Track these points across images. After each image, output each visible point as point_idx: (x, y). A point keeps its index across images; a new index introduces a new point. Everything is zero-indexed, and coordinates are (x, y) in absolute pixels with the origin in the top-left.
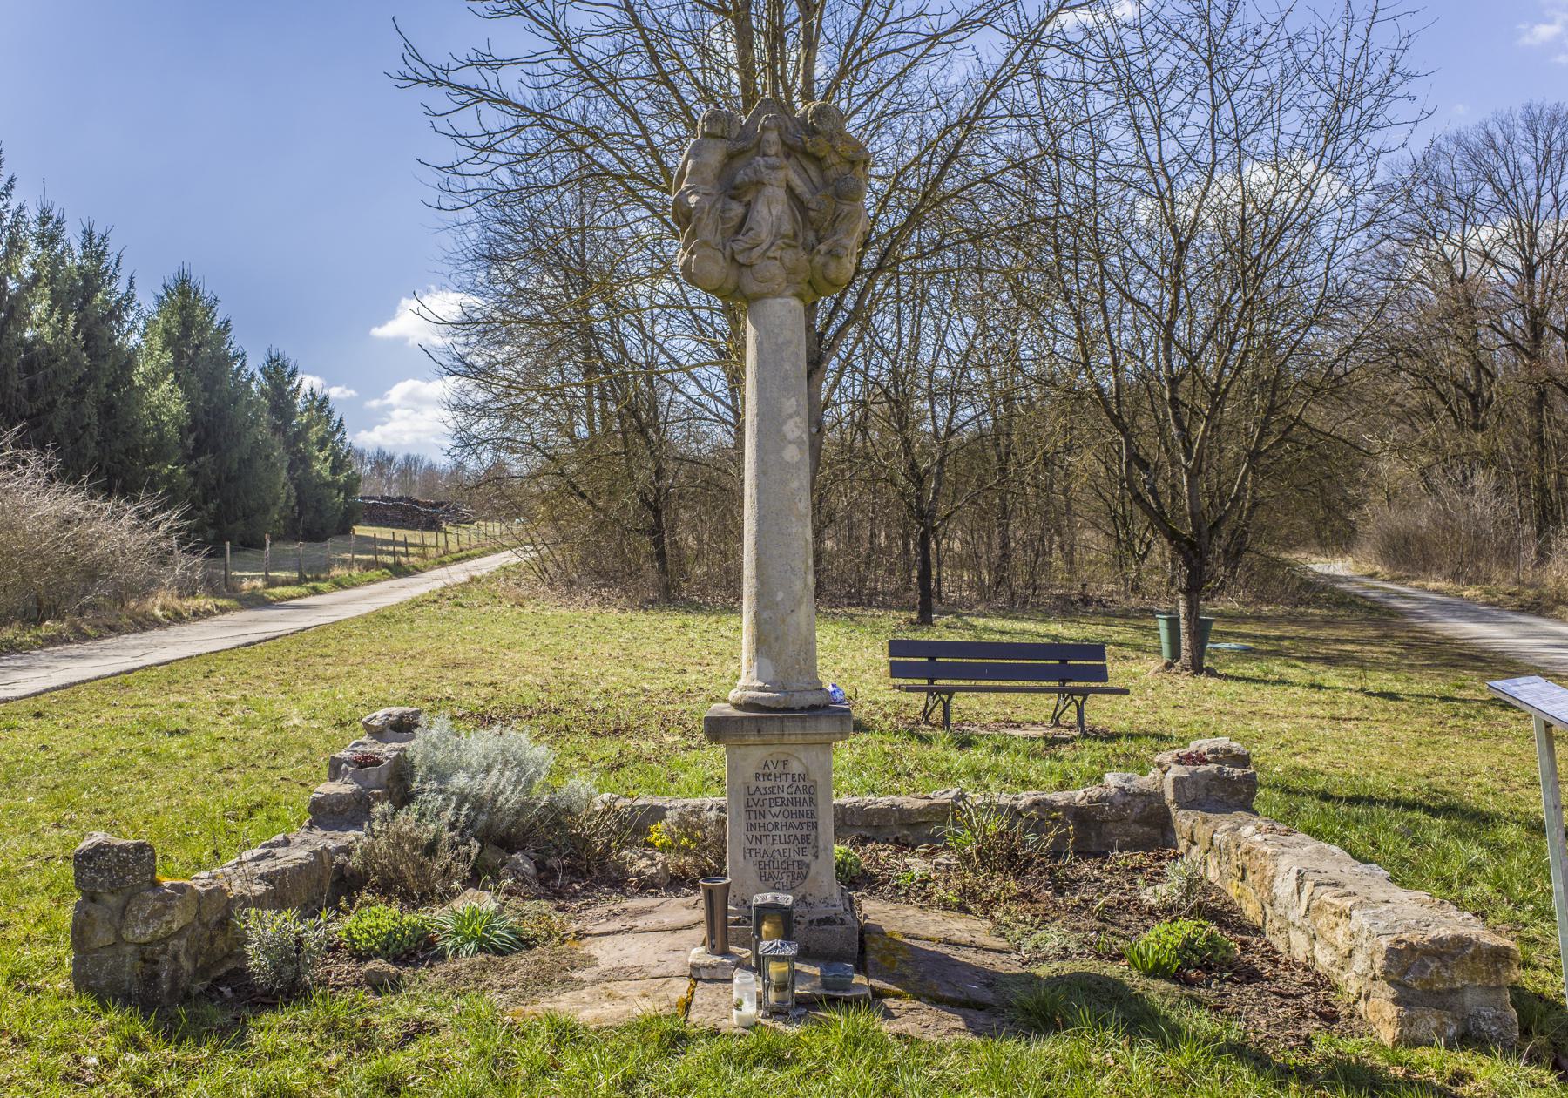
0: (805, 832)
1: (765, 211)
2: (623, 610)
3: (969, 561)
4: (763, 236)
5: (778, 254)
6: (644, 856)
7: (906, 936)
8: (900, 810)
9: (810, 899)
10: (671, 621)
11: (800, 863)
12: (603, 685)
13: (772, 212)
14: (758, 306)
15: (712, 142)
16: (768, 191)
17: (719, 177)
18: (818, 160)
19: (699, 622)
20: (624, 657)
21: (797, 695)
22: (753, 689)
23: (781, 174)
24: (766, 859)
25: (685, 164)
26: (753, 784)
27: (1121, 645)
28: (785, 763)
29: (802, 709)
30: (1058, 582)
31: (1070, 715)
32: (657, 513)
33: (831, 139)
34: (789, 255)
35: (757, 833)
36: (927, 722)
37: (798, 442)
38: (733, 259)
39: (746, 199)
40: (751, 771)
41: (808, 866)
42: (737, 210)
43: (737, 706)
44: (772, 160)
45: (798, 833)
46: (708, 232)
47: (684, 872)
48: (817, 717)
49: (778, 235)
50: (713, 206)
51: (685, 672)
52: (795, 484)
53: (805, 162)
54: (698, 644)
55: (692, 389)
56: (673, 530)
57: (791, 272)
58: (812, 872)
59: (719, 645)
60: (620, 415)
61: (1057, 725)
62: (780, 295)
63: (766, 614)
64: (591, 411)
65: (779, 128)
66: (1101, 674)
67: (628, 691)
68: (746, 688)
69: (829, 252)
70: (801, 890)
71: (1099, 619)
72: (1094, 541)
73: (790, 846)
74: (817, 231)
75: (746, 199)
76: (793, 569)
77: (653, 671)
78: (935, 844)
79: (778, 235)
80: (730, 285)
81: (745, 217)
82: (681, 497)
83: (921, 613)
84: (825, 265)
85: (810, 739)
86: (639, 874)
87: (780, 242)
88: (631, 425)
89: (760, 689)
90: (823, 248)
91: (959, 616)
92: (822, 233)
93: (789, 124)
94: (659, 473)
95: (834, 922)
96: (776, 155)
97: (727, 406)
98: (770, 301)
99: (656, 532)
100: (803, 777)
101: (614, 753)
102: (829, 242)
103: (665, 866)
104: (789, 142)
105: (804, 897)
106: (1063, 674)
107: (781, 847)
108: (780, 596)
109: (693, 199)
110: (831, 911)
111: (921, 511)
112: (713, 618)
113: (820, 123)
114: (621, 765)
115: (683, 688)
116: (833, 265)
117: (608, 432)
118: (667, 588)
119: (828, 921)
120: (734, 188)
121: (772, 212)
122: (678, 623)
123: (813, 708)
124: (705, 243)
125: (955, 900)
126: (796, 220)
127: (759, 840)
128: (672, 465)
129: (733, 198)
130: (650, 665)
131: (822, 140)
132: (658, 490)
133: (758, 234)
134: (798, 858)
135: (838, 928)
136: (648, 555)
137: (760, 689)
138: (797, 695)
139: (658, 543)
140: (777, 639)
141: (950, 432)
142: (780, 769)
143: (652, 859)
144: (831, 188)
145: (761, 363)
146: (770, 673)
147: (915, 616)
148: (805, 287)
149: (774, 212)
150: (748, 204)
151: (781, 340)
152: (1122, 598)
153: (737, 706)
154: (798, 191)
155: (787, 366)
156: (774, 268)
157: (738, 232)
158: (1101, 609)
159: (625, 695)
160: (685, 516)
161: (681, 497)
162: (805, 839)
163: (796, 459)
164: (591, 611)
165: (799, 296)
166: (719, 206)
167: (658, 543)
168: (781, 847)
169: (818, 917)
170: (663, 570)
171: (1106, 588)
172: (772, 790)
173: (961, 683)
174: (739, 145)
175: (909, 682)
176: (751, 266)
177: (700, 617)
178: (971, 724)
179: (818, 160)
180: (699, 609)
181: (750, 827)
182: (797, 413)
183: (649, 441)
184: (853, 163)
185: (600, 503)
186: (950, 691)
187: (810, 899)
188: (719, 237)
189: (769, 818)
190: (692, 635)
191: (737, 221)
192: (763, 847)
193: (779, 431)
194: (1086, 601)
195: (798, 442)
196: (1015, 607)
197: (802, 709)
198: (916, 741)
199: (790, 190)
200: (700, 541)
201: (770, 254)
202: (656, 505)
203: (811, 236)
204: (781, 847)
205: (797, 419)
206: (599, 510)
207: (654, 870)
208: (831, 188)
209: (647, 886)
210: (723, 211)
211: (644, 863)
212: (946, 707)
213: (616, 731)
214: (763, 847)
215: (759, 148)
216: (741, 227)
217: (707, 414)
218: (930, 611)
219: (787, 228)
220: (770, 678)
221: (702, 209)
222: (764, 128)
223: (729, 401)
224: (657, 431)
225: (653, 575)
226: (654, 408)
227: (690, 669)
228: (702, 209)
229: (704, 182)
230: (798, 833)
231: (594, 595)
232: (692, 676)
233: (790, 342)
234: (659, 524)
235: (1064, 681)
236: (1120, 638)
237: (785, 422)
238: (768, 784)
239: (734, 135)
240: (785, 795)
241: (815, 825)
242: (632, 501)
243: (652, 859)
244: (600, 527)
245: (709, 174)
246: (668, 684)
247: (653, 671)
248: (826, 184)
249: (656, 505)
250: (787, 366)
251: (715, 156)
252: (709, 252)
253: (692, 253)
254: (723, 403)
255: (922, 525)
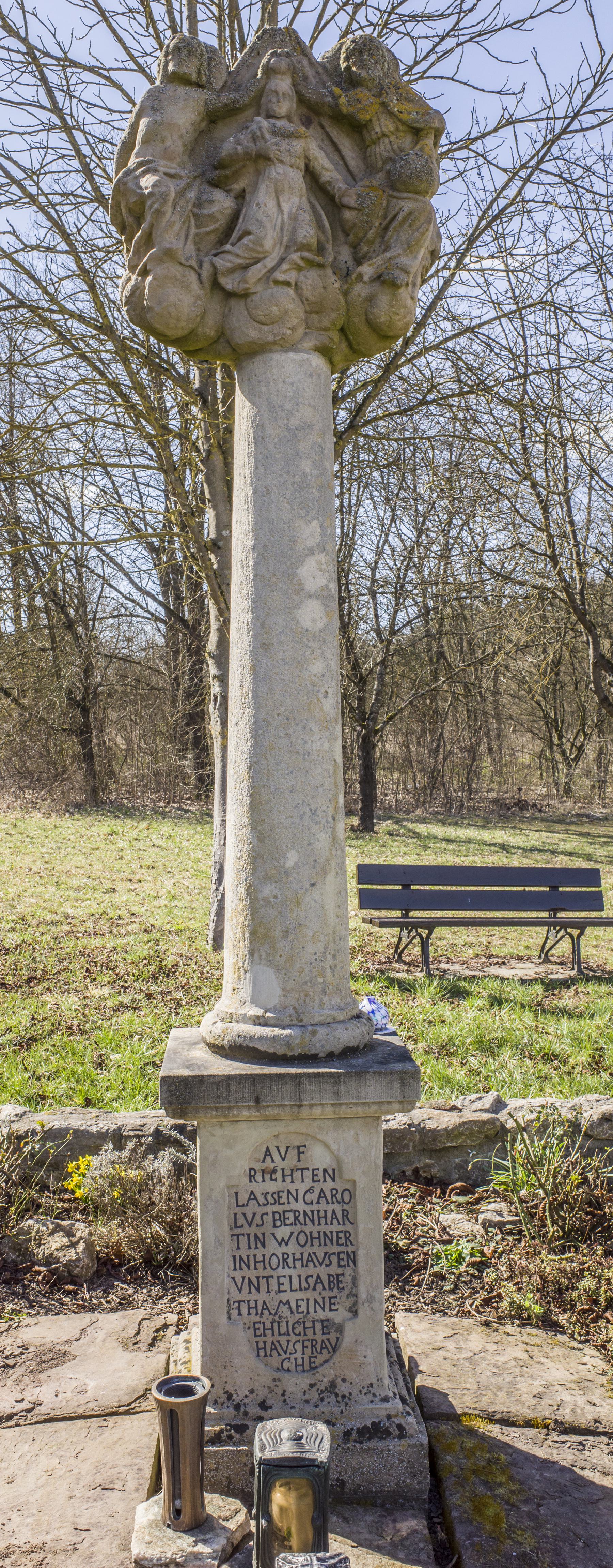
0: (334, 1269)
1: (271, 204)
2: (48, 815)
3: (406, 764)
4: (268, 244)
5: (292, 276)
6: (58, 1228)
7: (491, 1418)
8: (422, 1131)
9: (343, 1388)
10: (96, 828)
11: (327, 1325)
12: (20, 909)
13: (279, 207)
14: (257, 365)
15: (181, 90)
16: (276, 171)
17: (191, 150)
18: (357, 128)
19: (128, 828)
20: (48, 874)
21: (322, 1031)
22: (245, 1019)
23: (298, 146)
24: (267, 1318)
25: (134, 128)
26: (245, 1186)
27: (571, 854)
28: (300, 1150)
29: (330, 1057)
30: (488, 789)
31: (564, 947)
32: (85, 711)
33: (381, 91)
34: (311, 280)
35: (252, 1274)
36: (400, 960)
37: (321, 595)
38: (216, 284)
39: (237, 187)
40: (242, 1165)
41: (340, 1329)
42: (222, 202)
43: (217, 1049)
44: (281, 124)
45: (323, 1272)
46: (173, 235)
47: (118, 1254)
48: (360, 1074)
49: (294, 245)
50: (181, 194)
51: (114, 890)
52: (317, 667)
53: (335, 133)
54: (128, 855)
55: (124, 586)
56: (101, 730)
57: (314, 309)
58: (347, 1341)
59: (151, 856)
60: (47, 610)
61: (547, 961)
62: (293, 347)
63: (268, 890)
64: (17, 608)
65: (294, 72)
66: (596, 901)
67: (49, 917)
68: (231, 1018)
69: (379, 278)
70: (327, 1373)
71: (541, 825)
72: (525, 747)
73: (309, 1294)
74: (355, 247)
75: (237, 187)
76: (313, 812)
77: (78, 890)
78: (473, 1184)
79: (294, 245)
80: (209, 330)
81: (235, 217)
82: (110, 695)
83: (363, 819)
84: (370, 300)
85: (344, 1111)
86: (49, 1261)
87: (295, 256)
88: (60, 620)
89: (259, 1021)
90: (367, 270)
91: (397, 822)
92: (364, 248)
93: (310, 73)
94: (88, 671)
95: (387, 1433)
96: (289, 117)
97: (160, 603)
98: (278, 357)
99: (83, 732)
100: (332, 1174)
101: (23, 1019)
102: (378, 261)
103: (89, 1245)
104: (310, 95)
105: (333, 1384)
106: (554, 902)
107: (292, 1297)
108: (292, 859)
109: (147, 182)
110: (381, 1410)
111: (363, 713)
112: (144, 825)
113: (363, 66)
114: (33, 1039)
115: (113, 914)
116: (384, 299)
117: (34, 628)
118: (94, 791)
119: (376, 1431)
120: (219, 166)
121: (279, 207)
122: (106, 830)
123: (348, 1052)
124: (169, 254)
125: (537, 1309)
126: (320, 227)
127: (254, 1285)
128: (102, 663)
129: (215, 184)
130: (75, 882)
131: (364, 95)
132: (86, 688)
133: (259, 242)
134: (321, 1315)
135: (394, 1445)
136: (74, 757)
137: (259, 1021)
138: (322, 1031)
139: (86, 743)
140: (286, 933)
141: (393, 633)
142: (291, 1160)
143: (69, 1234)
144: (381, 176)
145: (262, 461)
146: (274, 994)
147: (355, 821)
148: (336, 336)
149: (286, 207)
150: (241, 196)
151: (294, 422)
152: (555, 802)
153: (217, 1049)
154: (326, 176)
155: (306, 466)
156: (286, 299)
157: (222, 242)
158: (538, 815)
159: (46, 924)
160: (114, 715)
161: (110, 695)
162: (335, 1281)
163: (320, 625)
164: (12, 816)
165: (324, 351)
166: (192, 195)
167: (86, 743)
168: (292, 1295)
169: (357, 1424)
170: (91, 773)
171: (536, 791)
172: (277, 1197)
173: (439, 914)
174: (226, 97)
175: (383, 913)
176: (245, 296)
177: (129, 822)
178: (449, 960)
179: (357, 128)
180: (129, 813)
181: (239, 1262)
182: (321, 547)
183: (77, 637)
184: (417, 133)
185: (25, 702)
186: (431, 925)
187: (343, 1388)
188: (190, 248)
189: (272, 1247)
190: (121, 845)
191: (222, 222)
192: (262, 1296)
193: (291, 575)
194: (522, 805)
195: (321, 595)
196: (454, 812)
197: (330, 1057)
198: (394, 991)
199: (311, 175)
200: (129, 741)
201: (280, 276)
202: (84, 704)
203: (345, 255)
204: (292, 1295)
205: (322, 557)
206: (23, 707)
207: (72, 1254)
208: (381, 176)
209: (65, 1285)
210: (198, 204)
211: (57, 1241)
212: (425, 945)
213: (30, 980)
214: (262, 1296)
215: (259, 102)
216: (229, 231)
217: (140, 612)
218: (371, 817)
219: (307, 233)
220: (275, 1001)
221: (164, 196)
222: (269, 71)
223: (160, 598)
224: (86, 627)
225: (79, 777)
226: (83, 603)
227: (119, 886)
228: (164, 196)
229: (167, 155)
230: (323, 1272)
231: (17, 797)
232: (121, 898)
233: (309, 427)
234: (87, 724)
235: (556, 911)
236: (569, 847)
237: (301, 561)
238: (271, 1187)
239: (218, 84)
240: (301, 1206)
241: (353, 1258)
242: (60, 701)
243: (69, 1234)
244: (24, 726)
245: (176, 144)
246: (96, 909)
247: (78, 890)
248: (370, 168)
249: (84, 704)
250: (306, 466)
251: (185, 111)
252: (175, 270)
253: (144, 273)
254: (155, 599)
255: (363, 727)
